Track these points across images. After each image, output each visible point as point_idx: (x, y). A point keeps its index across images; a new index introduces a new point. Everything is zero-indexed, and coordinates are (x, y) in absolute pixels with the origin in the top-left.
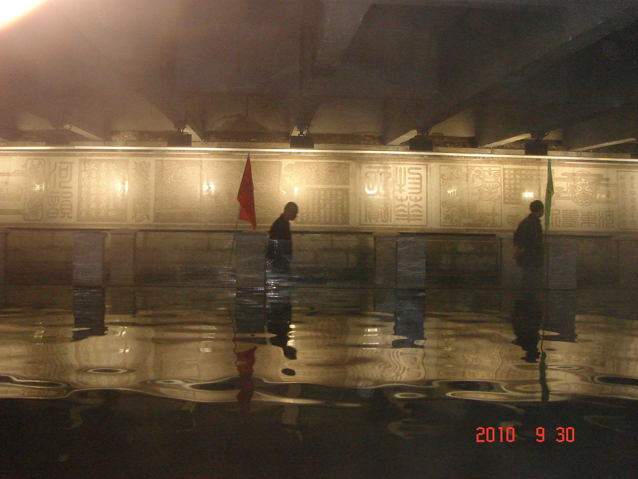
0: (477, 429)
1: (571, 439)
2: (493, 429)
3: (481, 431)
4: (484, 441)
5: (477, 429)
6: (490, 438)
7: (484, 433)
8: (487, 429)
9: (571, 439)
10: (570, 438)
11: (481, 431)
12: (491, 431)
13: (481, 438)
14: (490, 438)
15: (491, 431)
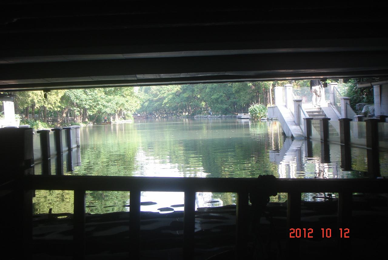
0: (290, 230)
2: (300, 230)
3: (292, 231)
4: (294, 237)
5: (290, 230)
6: (298, 235)
7: (294, 232)
8: (296, 230)
10: (329, 235)
11: (292, 231)
12: (298, 231)
13: (292, 235)
14: (298, 235)
15: (298, 231)
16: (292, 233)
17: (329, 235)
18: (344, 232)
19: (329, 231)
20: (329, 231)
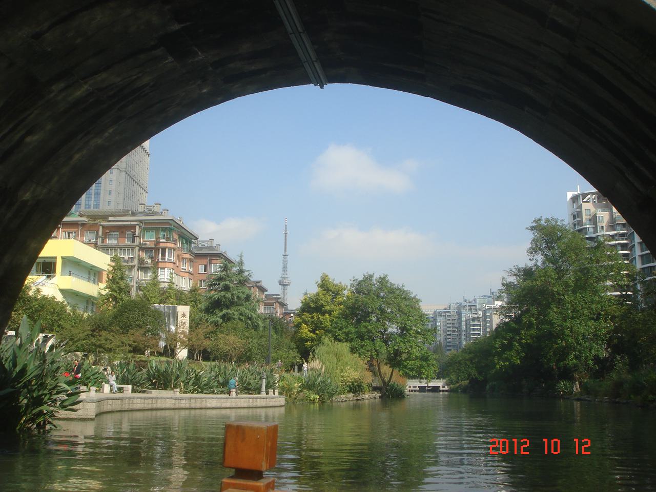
1: (557, 451)
2: (559, 441)
9: (557, 451)
10: (556, 450)
16: (585, 446)
17: (556, 450)
18: (581, 444)
19: (556, 443)
20: (556, 443)
